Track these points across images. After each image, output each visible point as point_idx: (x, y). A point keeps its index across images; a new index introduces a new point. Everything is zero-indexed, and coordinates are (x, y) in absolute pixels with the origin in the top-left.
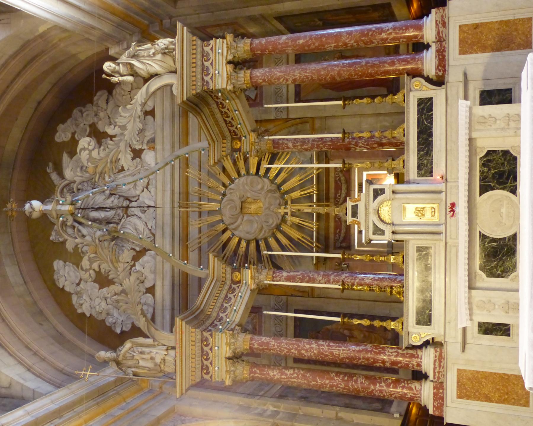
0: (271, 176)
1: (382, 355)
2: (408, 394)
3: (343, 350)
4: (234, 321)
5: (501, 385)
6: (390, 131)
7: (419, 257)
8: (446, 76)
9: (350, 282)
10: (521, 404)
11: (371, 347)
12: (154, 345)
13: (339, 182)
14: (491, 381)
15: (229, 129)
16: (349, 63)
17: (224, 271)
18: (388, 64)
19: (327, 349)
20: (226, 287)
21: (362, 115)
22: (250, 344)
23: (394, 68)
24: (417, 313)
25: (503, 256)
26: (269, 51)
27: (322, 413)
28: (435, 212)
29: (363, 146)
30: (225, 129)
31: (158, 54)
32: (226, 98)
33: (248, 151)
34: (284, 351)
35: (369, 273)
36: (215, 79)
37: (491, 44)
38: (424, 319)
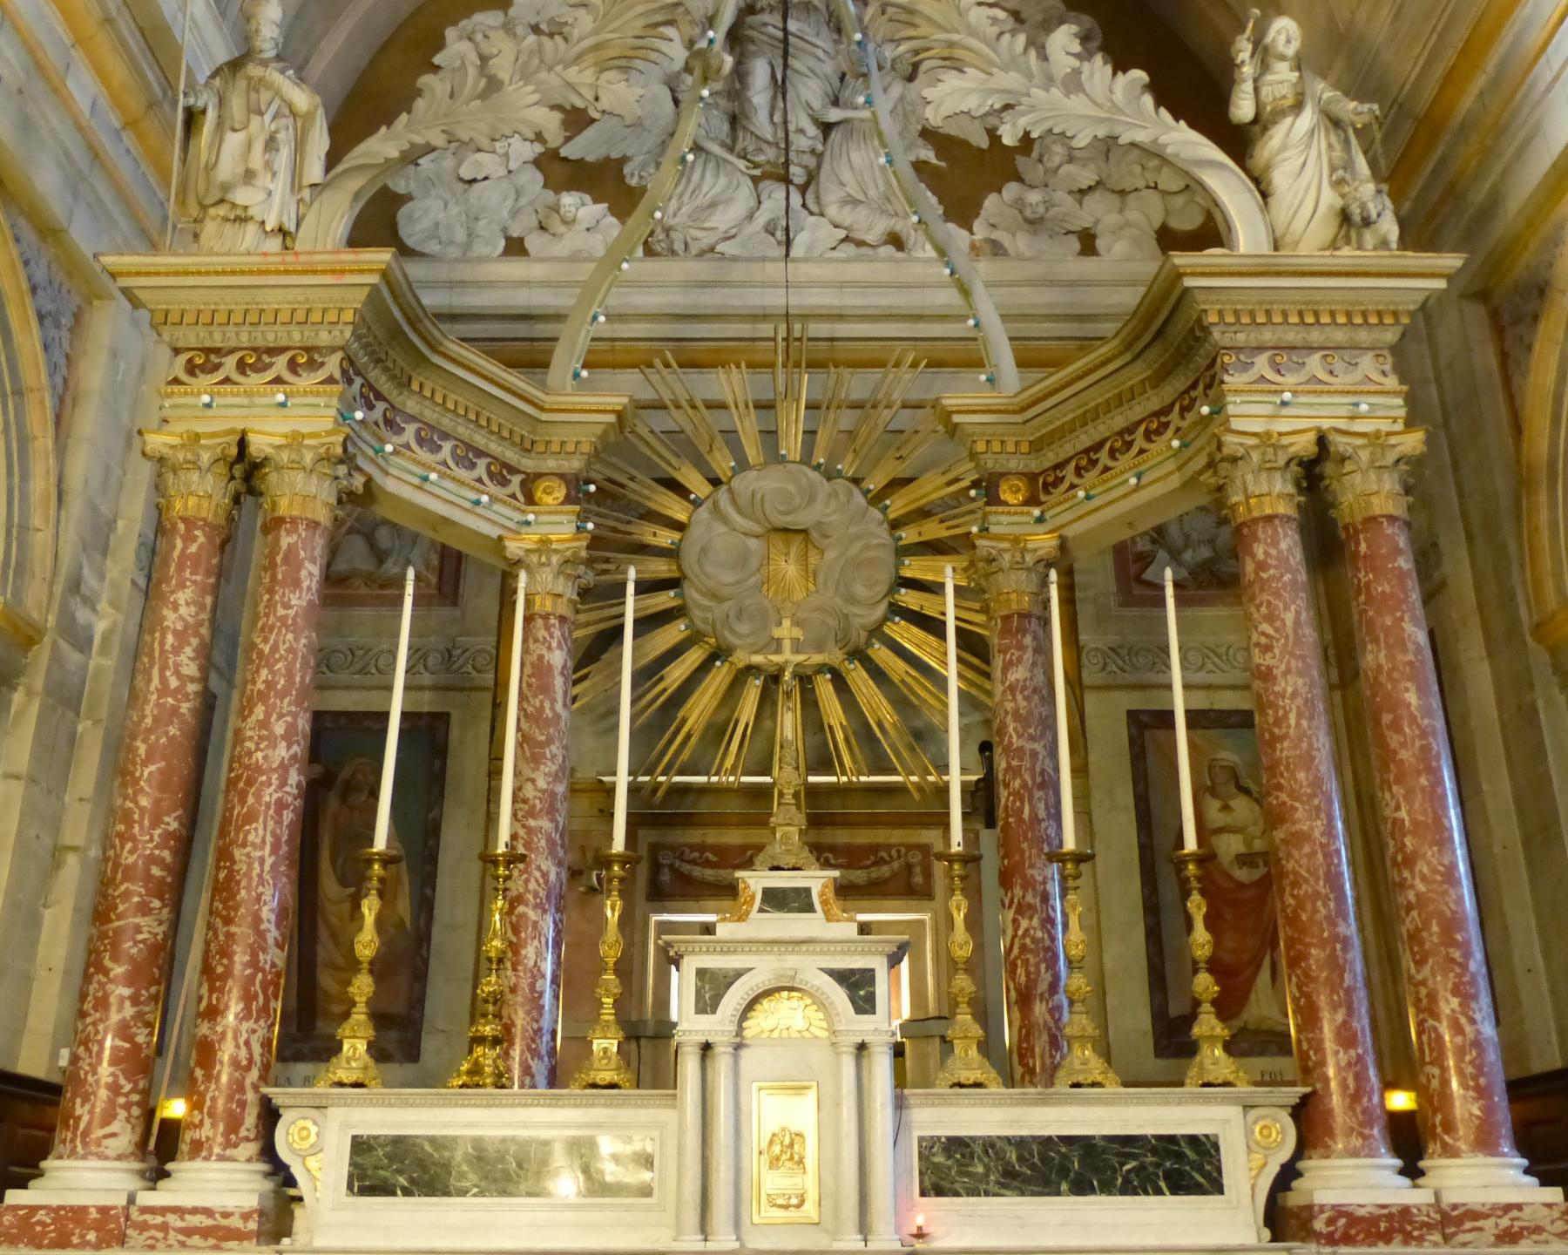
1: (241, 1006)
2: (87, 1107)
3: (262, 860)
4: (387, 473)
6: (1090, 1031)
11: (273, 965)
12: (300, 188)
15: (1067, 461)
16: (1341, 874)
17: (570, 448)
18: (1345, 1023)
19: (267, 798)
20: (511, 456)
21: (1100, 934)
22: (294, 520)
23: (1329, 1045)
24: (398, 1141)
26: (1368, 584)
28: (786, 1207)
29: (1020, 932)
30: (1068, 449)
31: (1343, 196)
32: (1189, 439)
33: (993, 529)
34: (266, 640)
35: (559, 956)
36: (1262, 391)
38: (376, 1168)
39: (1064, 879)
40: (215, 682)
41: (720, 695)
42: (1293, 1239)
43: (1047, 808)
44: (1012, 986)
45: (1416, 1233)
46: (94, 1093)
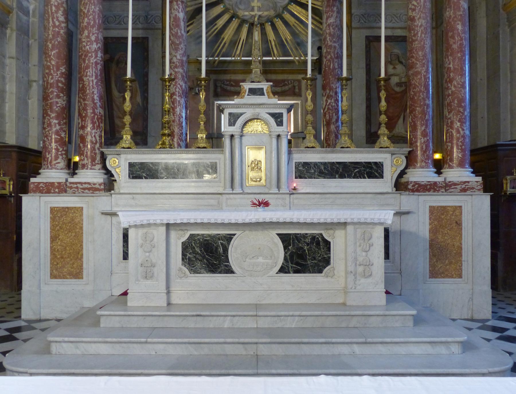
0: (292, 7)
1: (91, 125)
2: (50, 155)
3: (93, 81)
5: (71, 251)
7: (206, 165)
8: (407, 193)
9: (176, 91)
10: (53, 271)
11: (100, 113)
13: (283, 84)
14: (73, 241)
18: (425, 130)
19: (92, 61)
24: (142, 164)
25: (207, 260)
27: (34, 66)
28: (256, 181)
29: (328, 104)
34: (85, 8)
37: (438, 238)
38: (136, 171)
39: (342, 86)
40: (70, 26)
41: (235, 30)
42: (402, 191)
43: (338, 65)
44: (324, 120)
45: (437, 189)
46: (52, 151)
